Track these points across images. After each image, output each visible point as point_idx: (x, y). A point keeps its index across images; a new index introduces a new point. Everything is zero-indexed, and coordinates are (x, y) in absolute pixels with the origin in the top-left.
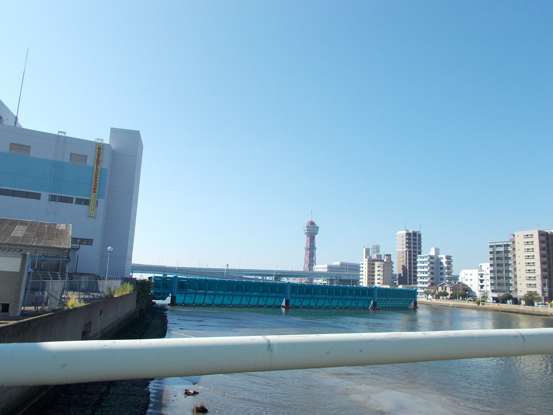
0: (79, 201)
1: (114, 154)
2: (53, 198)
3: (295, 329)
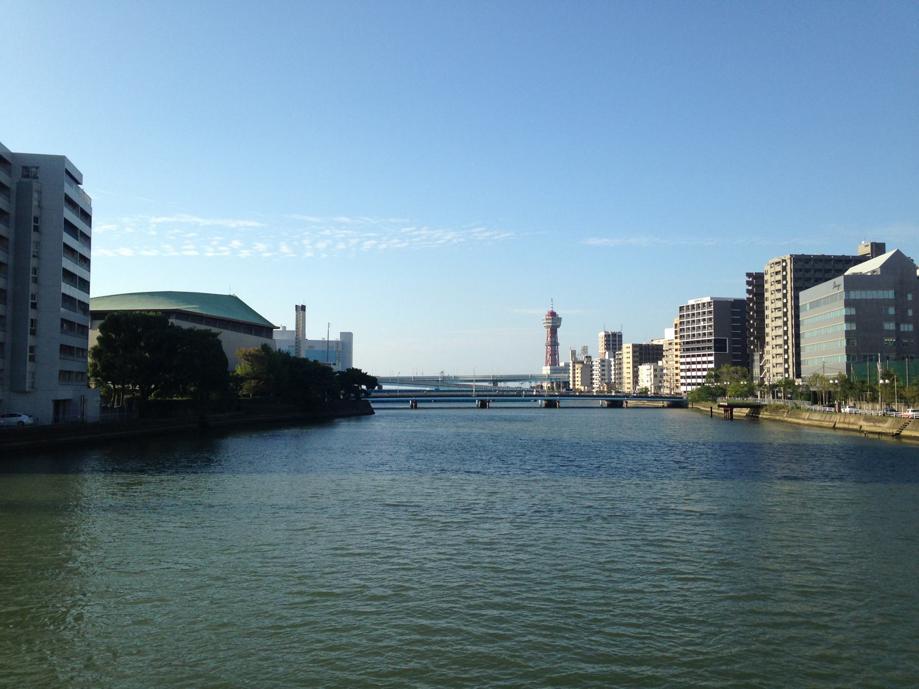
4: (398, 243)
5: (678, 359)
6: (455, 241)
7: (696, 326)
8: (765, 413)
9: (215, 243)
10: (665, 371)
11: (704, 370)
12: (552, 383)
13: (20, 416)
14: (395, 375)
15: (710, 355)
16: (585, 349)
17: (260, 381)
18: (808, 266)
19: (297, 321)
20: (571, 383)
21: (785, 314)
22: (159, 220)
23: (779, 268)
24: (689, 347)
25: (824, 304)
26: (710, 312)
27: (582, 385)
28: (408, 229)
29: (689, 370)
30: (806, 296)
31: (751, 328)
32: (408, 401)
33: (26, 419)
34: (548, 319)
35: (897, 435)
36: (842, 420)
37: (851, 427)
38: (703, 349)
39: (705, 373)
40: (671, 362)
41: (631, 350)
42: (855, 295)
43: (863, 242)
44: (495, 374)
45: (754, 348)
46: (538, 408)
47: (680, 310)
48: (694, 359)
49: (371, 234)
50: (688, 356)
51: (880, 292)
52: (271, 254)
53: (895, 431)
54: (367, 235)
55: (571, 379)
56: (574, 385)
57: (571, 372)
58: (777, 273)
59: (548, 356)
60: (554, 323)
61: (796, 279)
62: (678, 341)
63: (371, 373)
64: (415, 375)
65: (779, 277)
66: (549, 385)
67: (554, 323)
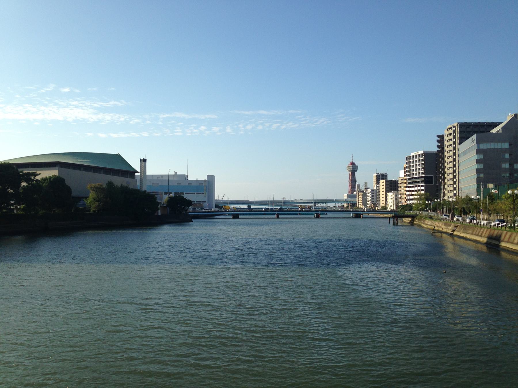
0: (202, 193)
1: (208, 181)
2: (197, 193)
3: (400, 239)
4: (293, 125)
6: (325, 123)
7: (414, 168)
9: (192, 128)
12: (348, 204)
14: (308, 200)
15: (422, 186)
16: (366, 184)
17: (101, 203)
19: (141, 167)
22: (164, 116)
24: (412, 181)
26: (422, 160)
27: (362, 205)
28: (299, 117)
29: (411, 195)
31: (440, 169)
34: (350, 167)
38: (421, 182)
39: (416, 197)
40: (403, 189)
42: (484, 146)
43: (510, 114)
45: (441, 181)
46: (350, 218)
50: (410, 187)
51: (500, 144)
52: (221, 133)
54: (276, 121)
56: (358, 205)
57: (357, 197)
59: (350, 188)
60: (354, 168)
64: (269, 200)
66: (347, 205)
67: (354, 168)
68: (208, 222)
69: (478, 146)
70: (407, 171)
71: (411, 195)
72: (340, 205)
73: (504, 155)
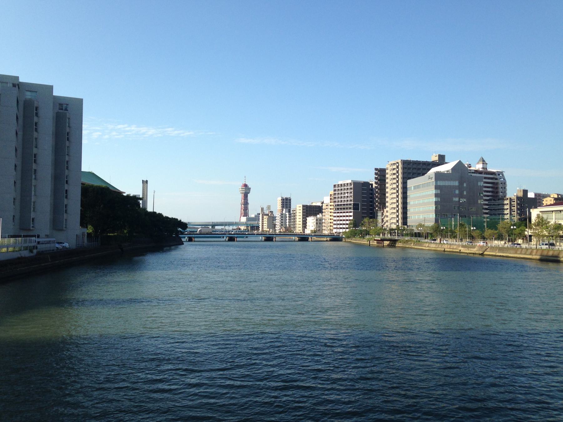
5: (332, 214)
7: (343, 196)
8: (400, 244)
10: (323, 221)
11: (347, 220)
12: (247, 227)
13: (64, 243)
15: (350, 212)
16: (269, 207)
18: (409, 166)
19: (143, 190)
20: (261, 227)
21: (398, 191)
23: (395, 167)
24: (339, 208)
25: (422, 187)
30: (411, 183)
32: (223, 237)
33: (66, 245)
34: (243, 189)
35: (482, 254)
36: (449, 247)
37: (454, 250)
40: (328, 216)
41: (301, 208)
44: (213, 221)
47: (334, 187)
48: (341, 214)
49: (97, 128)
50: (338, 213)
53: (481, 252)
55: (261, 225)
57: (261, 220)
58: (394, 169)
59: (242, 211)
60: (246, 190)
61: (403, 173)
62: (332, 204)
63: (184, 220)
65: (395, 172)
67: (246, 190)
68: (192, 244)
69: (436, 183)
70: (335, 198)
71: (338, 220)
72: (235, 227)
73: (455, 191)
